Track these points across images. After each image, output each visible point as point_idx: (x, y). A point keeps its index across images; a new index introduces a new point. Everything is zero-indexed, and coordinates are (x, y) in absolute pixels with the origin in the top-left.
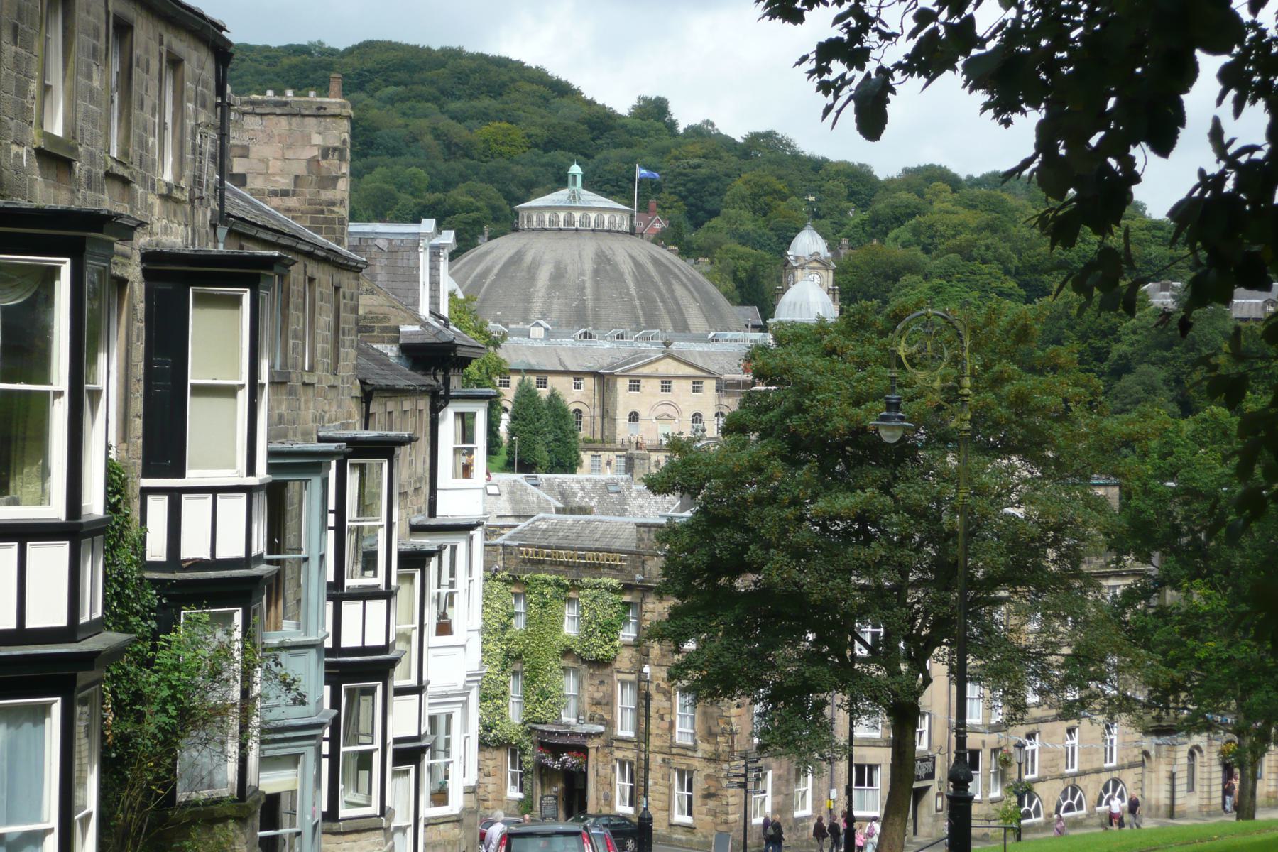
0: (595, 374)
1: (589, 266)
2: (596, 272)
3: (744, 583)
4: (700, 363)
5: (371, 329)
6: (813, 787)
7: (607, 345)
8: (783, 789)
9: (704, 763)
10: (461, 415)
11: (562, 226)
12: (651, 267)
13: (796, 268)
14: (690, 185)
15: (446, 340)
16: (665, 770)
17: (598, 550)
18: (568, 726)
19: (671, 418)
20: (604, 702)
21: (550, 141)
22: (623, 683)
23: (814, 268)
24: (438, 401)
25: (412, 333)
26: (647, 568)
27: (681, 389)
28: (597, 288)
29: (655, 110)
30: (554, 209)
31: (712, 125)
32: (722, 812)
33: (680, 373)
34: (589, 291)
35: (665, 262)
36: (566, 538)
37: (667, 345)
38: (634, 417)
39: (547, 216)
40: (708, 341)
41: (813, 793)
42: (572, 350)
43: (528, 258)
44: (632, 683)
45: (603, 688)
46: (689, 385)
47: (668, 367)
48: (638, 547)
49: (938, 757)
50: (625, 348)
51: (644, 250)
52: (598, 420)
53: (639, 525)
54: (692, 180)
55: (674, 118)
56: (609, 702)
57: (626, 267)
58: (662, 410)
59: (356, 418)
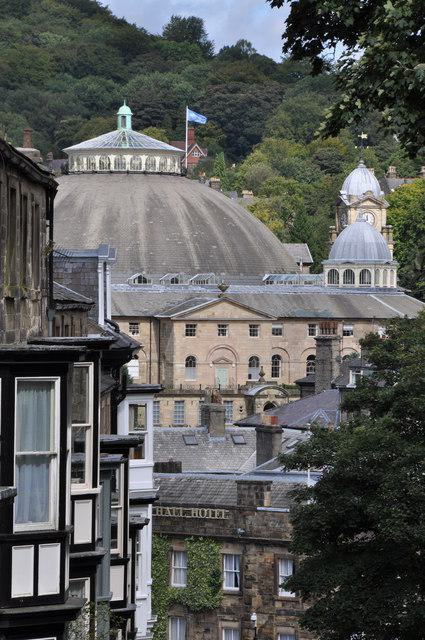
0: (150, 319)
1: (141, 209)
2: (149, 216)
3: (364, 536)
4: (255, 306)
7: (162, 289)
10: (134, 407)
11: (112, 168)
12: (204, 210)
13: (349, 207)
14: (228, 110)
15: (122, 345)
17: (201, 506)
19: (228, 362)
21: (80, 64)
22: (228, 630)
23: (368, 207)
26: (248, 523)
27: (238, 333)
28: (151, 232)
29: (188, 31)
30: (104, 151)
31: (249, 45)
33: (236, 317)
34: (142, 235)
35: (217, 204)
37: (223, 289)
38: (191, 362)
39: (97, 158)
40: (262, 284)
42: (127, 295)
43: (80, 202)
44: (235, 630)
46: (245, 329)
47: (224, 311)
48: (239, 502)
50: (179, 293)
51: (200, 192)
52: (155, 365)
53: (239, 483)
54: (230, 105)
55: (209, 38)
57: (179, 210)
58: (219, 354)
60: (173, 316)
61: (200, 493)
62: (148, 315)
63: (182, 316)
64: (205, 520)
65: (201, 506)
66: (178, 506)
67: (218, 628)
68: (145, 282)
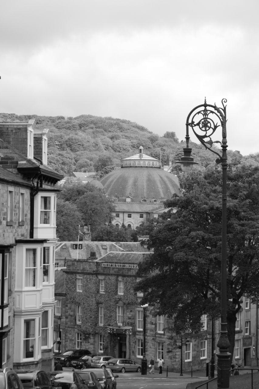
1: (145, 178)
5: (7, 163)
6: (207, 348)
8: (196, 349)
9: (167, 340)
16: (153, 342)
17: (116, 263)
18: (120, 327)
20: (132, 318)
24: (34, 192)
25: (22, 164)
32: (174, 358)
36: (119, 260)
41: (207, 351)
45: (132, 313)
49: (253, 337)
56: (134, 318)
59: (89, 235)
60: (154, 212)
61: (130, 259)
62: (146, 211)
63: (157, 212)
64: (131, 269)
65: (129, 263)
66: (121, 263)
67: (135, 310)
68: (146, 201)
